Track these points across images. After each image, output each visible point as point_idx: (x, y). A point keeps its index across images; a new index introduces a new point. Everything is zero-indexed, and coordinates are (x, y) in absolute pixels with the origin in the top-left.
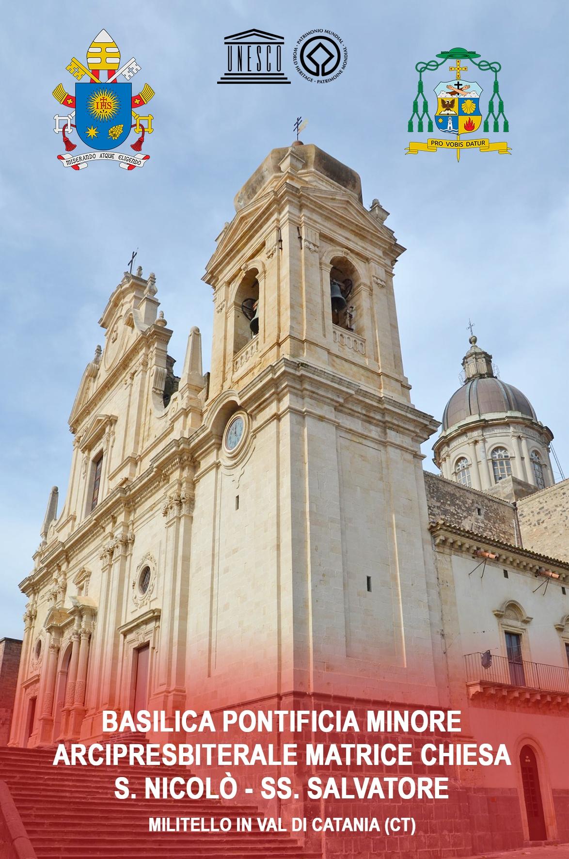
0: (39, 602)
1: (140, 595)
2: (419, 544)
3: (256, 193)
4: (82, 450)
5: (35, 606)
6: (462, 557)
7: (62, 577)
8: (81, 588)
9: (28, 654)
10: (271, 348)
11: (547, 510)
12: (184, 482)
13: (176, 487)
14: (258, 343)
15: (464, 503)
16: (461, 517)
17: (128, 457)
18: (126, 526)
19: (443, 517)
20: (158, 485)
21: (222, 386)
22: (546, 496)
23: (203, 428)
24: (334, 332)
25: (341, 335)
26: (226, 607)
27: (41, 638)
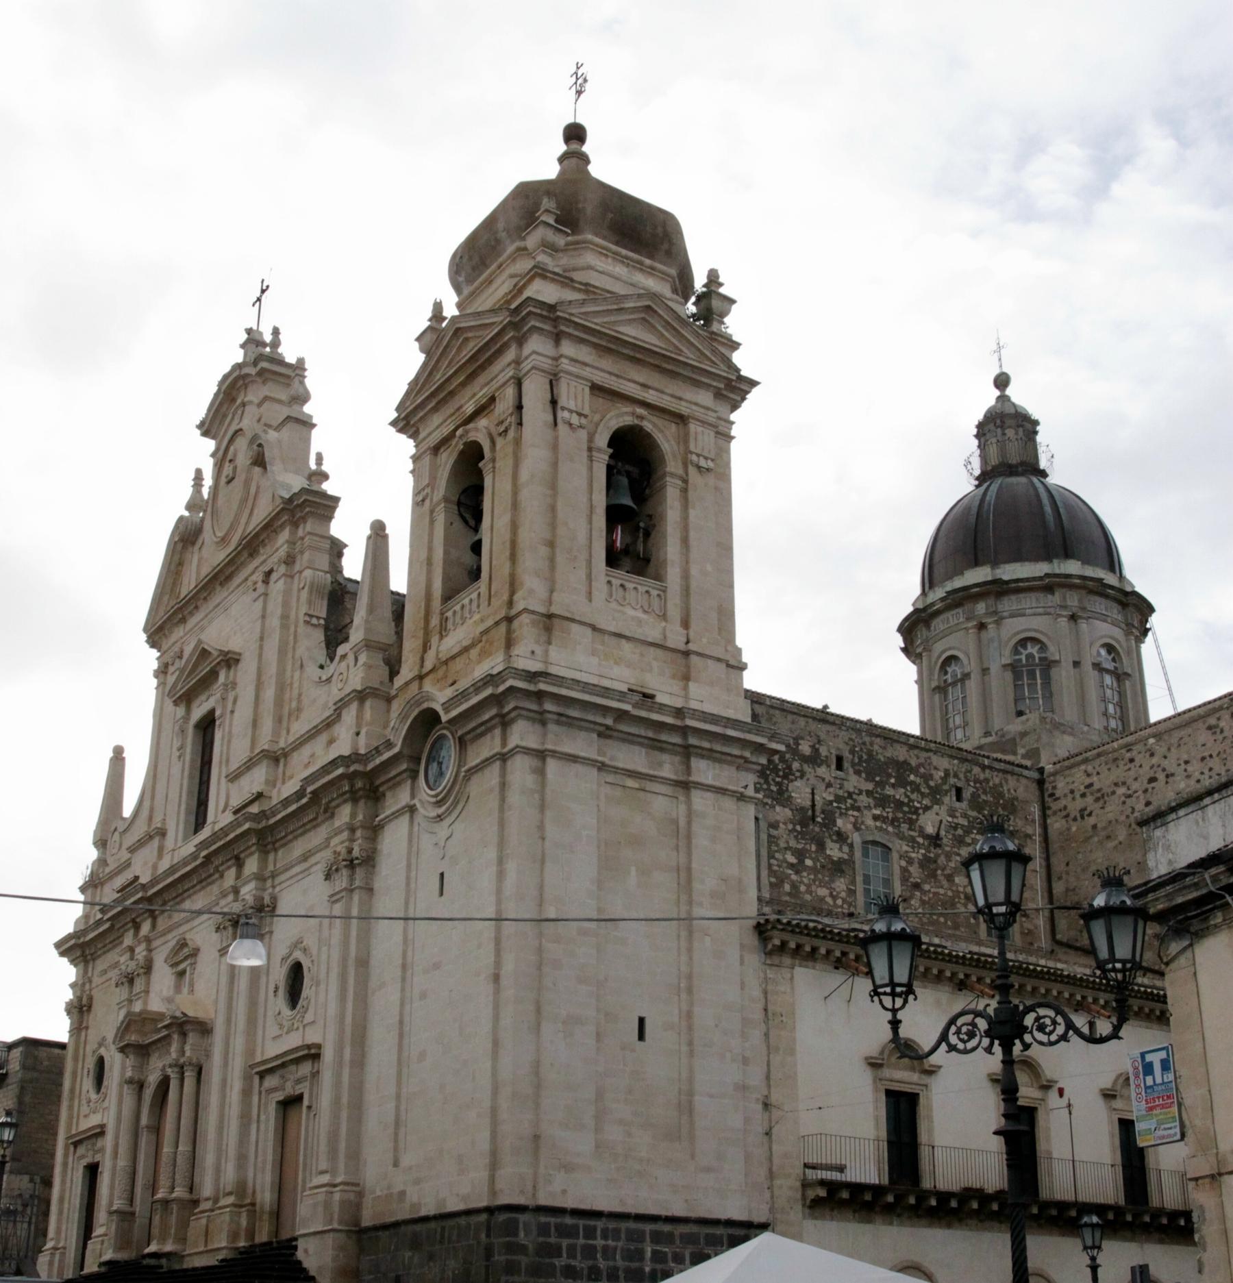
0: (96, 980)
1: (287, 1012)
2: (734, 954)
3: (487, 267)
4: (175, 701)
5: (87, 987)
6: (814, 968)
7: (143, 946)
8: (182, 974)
9: (79, 1079)
10: (497, 623)
11: (1099, 790)
12: (358, 828)
13: (345, 835)
14: (479, 594)
15: (927, 778)
16: (917, 809)
17: (262, 751)
18: (260, 878)
19: (877, 812)
20: (315, 819)
21: (422, 660)
22: (1097, 762)
23: (389, 745)
24: (609, 582)
25: (622, 586)
26: (422, 1056)
27: (102, 1051)
